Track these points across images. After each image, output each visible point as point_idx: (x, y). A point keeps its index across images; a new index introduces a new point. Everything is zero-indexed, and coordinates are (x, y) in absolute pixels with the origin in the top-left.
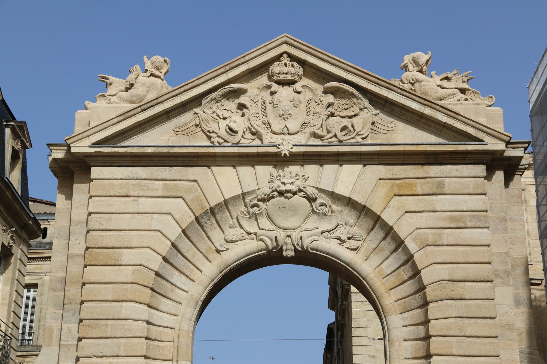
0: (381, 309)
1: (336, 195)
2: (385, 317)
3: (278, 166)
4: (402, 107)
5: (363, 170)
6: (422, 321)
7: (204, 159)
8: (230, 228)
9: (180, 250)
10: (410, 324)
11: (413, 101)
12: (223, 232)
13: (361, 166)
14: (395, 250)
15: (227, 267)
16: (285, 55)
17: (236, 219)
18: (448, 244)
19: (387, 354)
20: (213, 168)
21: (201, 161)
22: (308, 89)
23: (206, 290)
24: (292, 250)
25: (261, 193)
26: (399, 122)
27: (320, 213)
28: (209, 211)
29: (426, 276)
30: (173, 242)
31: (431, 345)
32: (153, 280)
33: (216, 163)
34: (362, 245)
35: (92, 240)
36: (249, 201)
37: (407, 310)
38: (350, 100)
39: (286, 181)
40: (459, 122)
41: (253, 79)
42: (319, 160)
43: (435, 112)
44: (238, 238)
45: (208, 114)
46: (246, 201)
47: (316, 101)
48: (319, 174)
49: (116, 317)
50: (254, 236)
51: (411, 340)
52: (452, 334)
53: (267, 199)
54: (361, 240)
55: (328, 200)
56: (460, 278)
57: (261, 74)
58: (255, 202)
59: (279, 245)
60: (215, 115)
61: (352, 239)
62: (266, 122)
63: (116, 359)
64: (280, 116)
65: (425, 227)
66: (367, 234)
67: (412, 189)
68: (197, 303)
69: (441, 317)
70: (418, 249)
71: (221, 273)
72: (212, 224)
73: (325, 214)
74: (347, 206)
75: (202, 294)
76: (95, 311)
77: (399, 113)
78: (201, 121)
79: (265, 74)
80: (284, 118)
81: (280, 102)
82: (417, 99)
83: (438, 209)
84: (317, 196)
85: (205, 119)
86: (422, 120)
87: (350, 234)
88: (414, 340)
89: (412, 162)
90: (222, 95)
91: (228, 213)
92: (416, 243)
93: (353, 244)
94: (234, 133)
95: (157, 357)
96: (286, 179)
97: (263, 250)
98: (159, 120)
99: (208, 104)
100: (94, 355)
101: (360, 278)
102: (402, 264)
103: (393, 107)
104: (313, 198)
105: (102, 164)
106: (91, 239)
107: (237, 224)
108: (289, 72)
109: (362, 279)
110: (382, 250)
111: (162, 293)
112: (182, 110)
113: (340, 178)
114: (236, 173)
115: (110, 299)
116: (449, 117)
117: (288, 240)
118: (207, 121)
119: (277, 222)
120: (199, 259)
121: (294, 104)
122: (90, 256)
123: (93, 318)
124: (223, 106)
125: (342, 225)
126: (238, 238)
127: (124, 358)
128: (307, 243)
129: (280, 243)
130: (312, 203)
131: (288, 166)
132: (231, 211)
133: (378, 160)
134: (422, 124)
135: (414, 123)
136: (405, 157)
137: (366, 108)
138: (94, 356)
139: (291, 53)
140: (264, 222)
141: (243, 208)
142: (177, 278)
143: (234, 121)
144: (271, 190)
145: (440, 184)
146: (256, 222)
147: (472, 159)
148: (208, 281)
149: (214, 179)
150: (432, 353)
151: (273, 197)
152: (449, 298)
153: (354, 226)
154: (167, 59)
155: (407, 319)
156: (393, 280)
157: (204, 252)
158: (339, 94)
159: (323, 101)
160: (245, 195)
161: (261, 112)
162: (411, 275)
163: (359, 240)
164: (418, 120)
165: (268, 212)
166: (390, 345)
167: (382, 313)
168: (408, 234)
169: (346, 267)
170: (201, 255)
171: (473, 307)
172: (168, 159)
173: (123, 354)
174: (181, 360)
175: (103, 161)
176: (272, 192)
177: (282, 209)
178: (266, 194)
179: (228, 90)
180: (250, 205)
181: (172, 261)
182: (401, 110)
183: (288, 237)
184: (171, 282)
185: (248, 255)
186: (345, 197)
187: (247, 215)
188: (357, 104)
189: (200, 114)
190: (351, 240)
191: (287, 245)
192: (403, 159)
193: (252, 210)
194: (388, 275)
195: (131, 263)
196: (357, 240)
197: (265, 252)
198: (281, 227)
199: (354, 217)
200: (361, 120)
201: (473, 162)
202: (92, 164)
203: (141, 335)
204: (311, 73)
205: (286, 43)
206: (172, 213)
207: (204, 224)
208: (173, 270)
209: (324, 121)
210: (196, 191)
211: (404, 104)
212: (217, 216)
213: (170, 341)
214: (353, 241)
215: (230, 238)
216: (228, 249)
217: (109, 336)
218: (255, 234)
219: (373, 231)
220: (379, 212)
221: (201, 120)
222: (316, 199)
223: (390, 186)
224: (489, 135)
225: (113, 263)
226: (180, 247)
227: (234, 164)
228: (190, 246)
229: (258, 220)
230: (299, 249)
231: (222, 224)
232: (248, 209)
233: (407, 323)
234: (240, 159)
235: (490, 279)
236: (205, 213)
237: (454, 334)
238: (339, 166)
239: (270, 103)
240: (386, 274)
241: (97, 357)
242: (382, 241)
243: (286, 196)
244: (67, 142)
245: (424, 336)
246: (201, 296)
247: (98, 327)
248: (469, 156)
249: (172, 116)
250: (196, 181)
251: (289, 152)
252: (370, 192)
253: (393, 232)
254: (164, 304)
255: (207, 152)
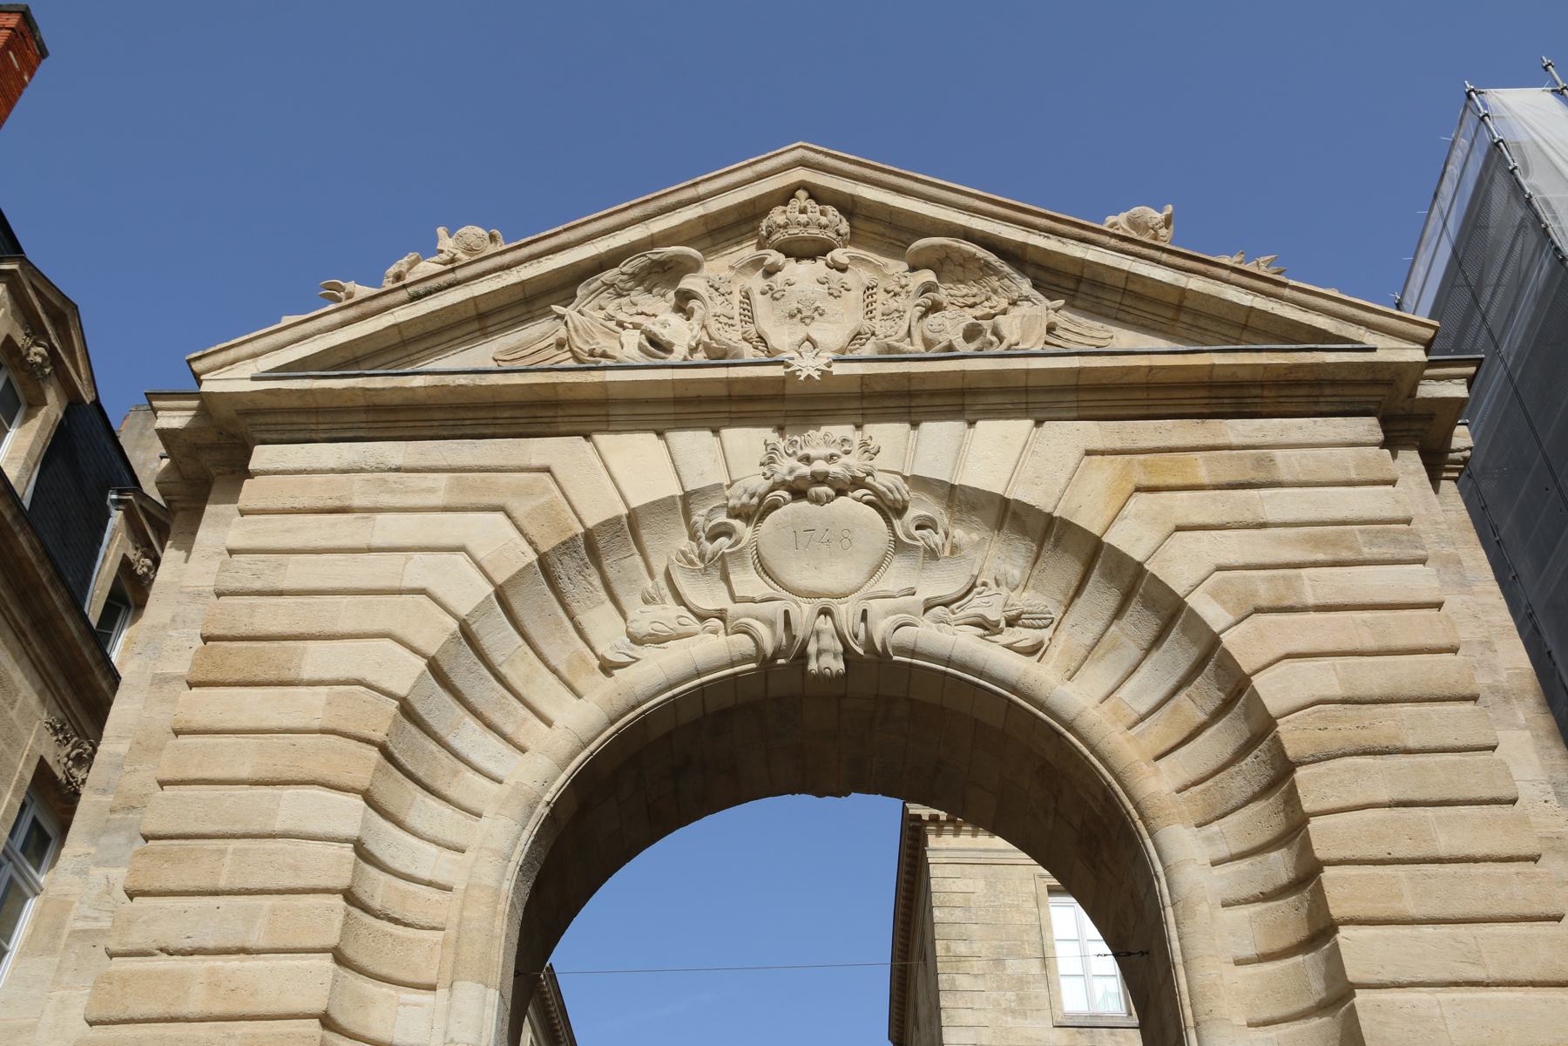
0: (1134, 813)
1: (964, 491)
2: (1151, 835)
3: (787, 429)
4: (1125, 289)
5: (1035, 434)
6: (1276, 834)
7: (576, 412)
8: (646, 602)
9: (487, 655)
10: (1235, 850)
11: (1155, 264)
12: (623, 614)
13: (1030, 423)
14: (1157, 641)
15: (633, 708)
16: (801, 194)
17: (663, 577)
18: (1322, 601)
19: (1173, 948)
20: (597, 437)
21: (566, 419)
22: (864, 268)
23: (563, 771)
24: (835, 656)
25: (740, 491)
26: (1120, 329)
27: (918, 547)
28: (581, 542)
29: (1273, 689)
30: (464, 620)
31: (1326, 889)
32: (389, 722)
33: (608, 426)
34: (1050, 640)
35: (219, 616)
36: (702, 519)
37: (1218, 813)
38: (980, 284)
39: (812, 452)
40: (1287, 305)
41: (717, 251)
42: (906, 410)
43: (1217, 285)
44: (667, 629)
45: (592, 317)
46: (695, 518)
47: (889, 289)
48: (909, 446)
49: (255, 828)
50: (717, 622)
51: (1247, 901)
52: (1390, 854)
53: (755, 512)
54: (1046, 627)
55: (941, 514)
56: (1377, 692)
57: (739, 239)
58: (722, 518)
59: (797, 639)
60: (612, 324)
61: (1020, 626)
62: (753, 335)
63: (237, 960)
64: (792, 316)
65: (1241, 562)
66: (1063, 608)
67: (1185, 472)
68: (532, 807)
69: (1342, 804)
70: (1231, 619)
71: (612, 723)
72: (589, 586)
73: (932, 554)
74: (996, 532)
75: (547, 783)
76: (190, 811)
77: (1117, 306)
78: (573, 334)
79: (750, 243)
80: (802, 320)
81: (789, 285)
82: (1165, 257)
83: (1270, 518)
84: (907, 497)
85: (584, 328)
86: (1183, 318)
87: (1013, 608)
88: (1254, 902)
89: (1173, 411)
90: (633, 276)
91: (638, 558)
92: (1223, 603)
93: (1024, 636)
94: (661, 351)
95: (384, 971)
96: (813, 447)
97: (745, 659)
98: (457, 333)
99: (593, 296)
100: (163, 945)
101: (1056, 725)
102: (1182, 678)
103: (1100, 294)
104: (896, 500)
105: (284, 437)
106: (219, 614)
107: (666, 592)
108: (814, 221)
109: (1062, 730)
110: (1114, 647)
111: (421, 773)
112: (523, 314)
113: (971, 451)
114: (665, 451)
115: (244, 772)
116: (1256, 296)
117: (825, 624)
118: (588, 333)
119: (788, 577)
120: (544, 689)
121: (829, 289)
122: (206, 658)
123: (180, 831)
124: (636, 305)
125: (984, 584)
126: (667, 629)
127: (264, 959)
128: (881, 629)
129: (800, 633)
130: (894, 521)
131: (817, 426)
132: (649, 551)
133: (1076, 405)
134: (1183, 330)
135: (1160, 331)
136: (1153, 395)
137: (1027, 299)
138: (162, 950)
139: (818, 183)
140: (748, 581)
141: (684, 543)
142: (469, 736)
143: (663, 324)
144: (770, 482)
145: (1262, 460)
146: (723, 585)
147: (1338, 399)
148: (570, 744)
149: (599, 464)
150: (1335, 917)
151: (775, 506)
152: (1354, 748)
153: (1021, 588)
154: (496, 232)
155: (1223, 840)
156: (1160, 731)
157: (562, 669)
158: (951, 271)
159: (907, 285)
160: (691, 501)
161: (737, 317)
162: (1218, 702)
163: (1040, 628)
164: (1172, 320)
165: (761, 549)
166: (1181, 918)
167: (1139, 823)
168: (1194, 581)
169: (1010, 700)
170: (551, 678)
171: (1439, 775)
172: (470, 415)
173: (263, 943)
174: (466, 980)
175: (288, 427)
176: (772, 490)
177: (804, 536)
178: (753, 491)
179: (649, 259)
180: (707, 530)
181: (459, 682)
182: (1122, 298)
183: (822, 617)
184: (452, 748)
185: (699, 674)
186: (991, 496)
187: (699, 563)
188: (1000, 290)
189: (570, 316)
190: (1017, 628)
191: (822, 636)
192: (1146, 403)
193: (710, 548)
194: (1142, 719)
195: (327, 676)
196: (1035, 628)
197: (753, 665)
198: (802, 588)
199: (1021, 561)
200: (1018, 321)
201: (1340, 409)
202: (258, 436)
203: (330, 884)
204: (873, 236)
205: (803, 163)
206: (471, 546)
207: (565, 585)
208: (462, 714)
209: (913, 324)
210: (546, 490)
211: (1131, 271)
212: (606, 563)
213: (435, 925)
214: (1021, 629)
215: (643, 626)
216: (638, 660)
217: (223, 884)
218: (721, 615)
219: (1079, 597)
220: (1097, 528)
221: (572, 329)
222: (905, 509)
223: (1120, 466)
224: (1374, 329)
225: (272, 675)
226: (487, 642)
227: (659, 427)
228: (520, 647)
229: (731, 577)
230: (860, 651)
231: (619, 589)
232: (699, 545)
233: (1223, 851)
234: (677, 411)
235: (1467, 692)
236: (567, 546)
237: (1396, 855)
238: (966, 426)
239: (763, 293)
240: (1135, 717)
241: (171, 955)
242: (1111, 623)
243: (814, 494)
244: (193, 366)
245: (1292, 875)
246: (546, 790)
247: (193, 857)
248: (1328, 391)
249: (493, 329)
250: (547, 470)
251: (819, 373)
252: (1063, 481)
253: (1148, 581)
254: (423, 810)
255: (580, 381)
